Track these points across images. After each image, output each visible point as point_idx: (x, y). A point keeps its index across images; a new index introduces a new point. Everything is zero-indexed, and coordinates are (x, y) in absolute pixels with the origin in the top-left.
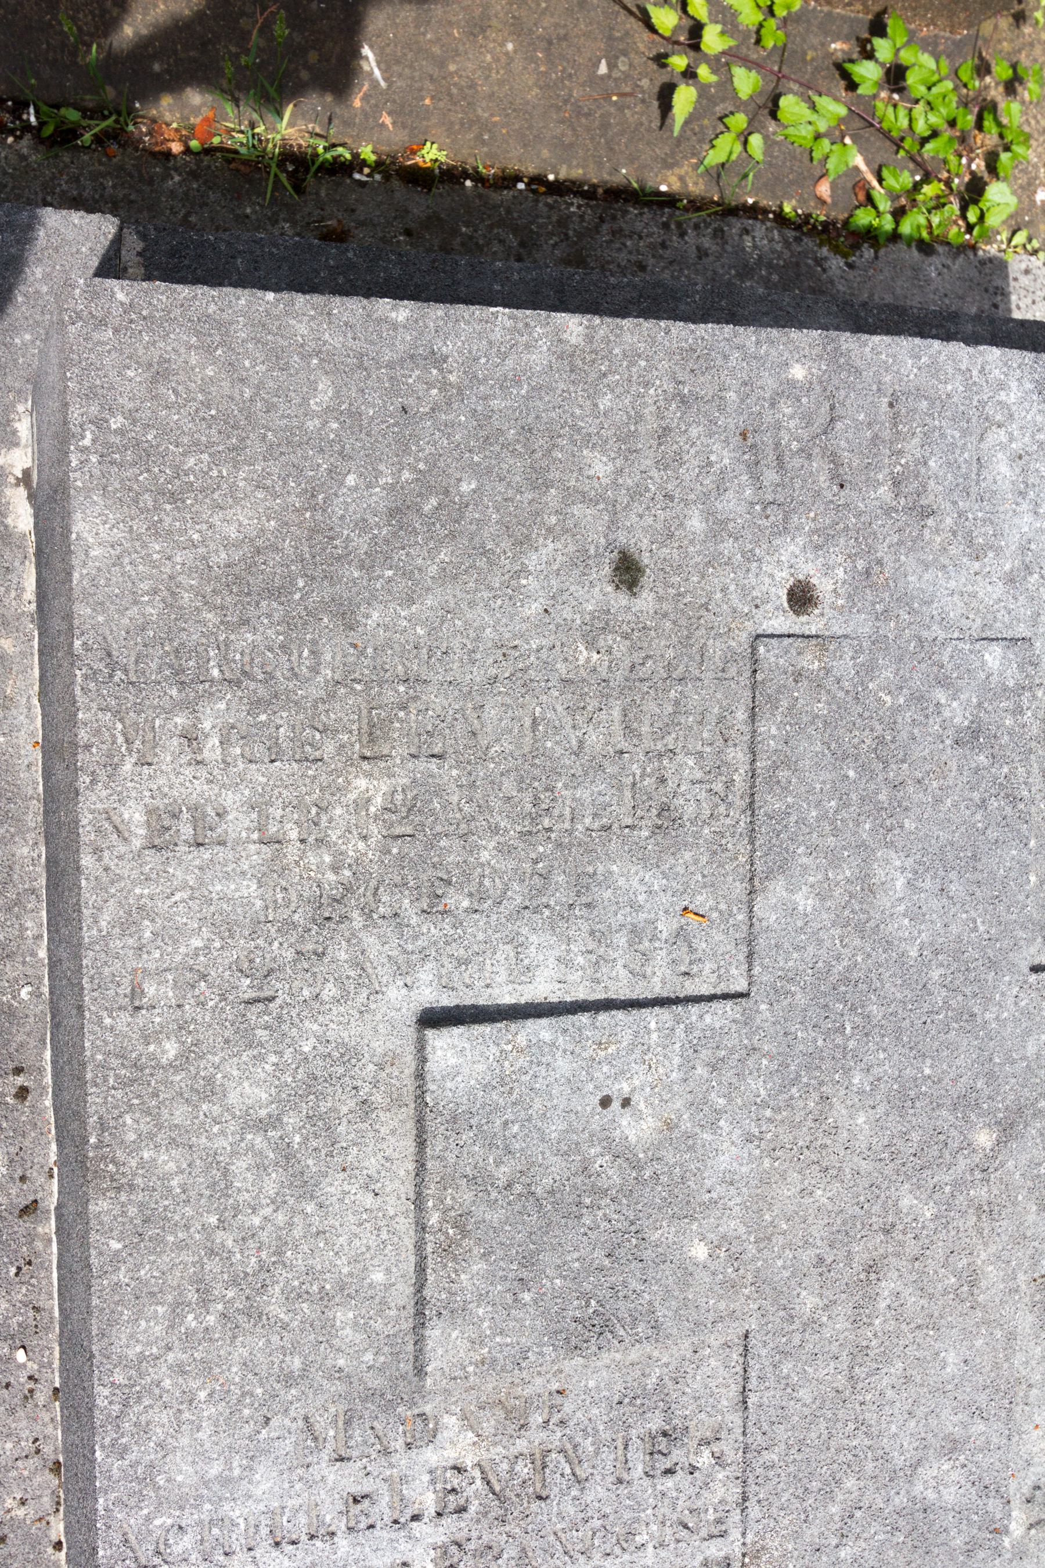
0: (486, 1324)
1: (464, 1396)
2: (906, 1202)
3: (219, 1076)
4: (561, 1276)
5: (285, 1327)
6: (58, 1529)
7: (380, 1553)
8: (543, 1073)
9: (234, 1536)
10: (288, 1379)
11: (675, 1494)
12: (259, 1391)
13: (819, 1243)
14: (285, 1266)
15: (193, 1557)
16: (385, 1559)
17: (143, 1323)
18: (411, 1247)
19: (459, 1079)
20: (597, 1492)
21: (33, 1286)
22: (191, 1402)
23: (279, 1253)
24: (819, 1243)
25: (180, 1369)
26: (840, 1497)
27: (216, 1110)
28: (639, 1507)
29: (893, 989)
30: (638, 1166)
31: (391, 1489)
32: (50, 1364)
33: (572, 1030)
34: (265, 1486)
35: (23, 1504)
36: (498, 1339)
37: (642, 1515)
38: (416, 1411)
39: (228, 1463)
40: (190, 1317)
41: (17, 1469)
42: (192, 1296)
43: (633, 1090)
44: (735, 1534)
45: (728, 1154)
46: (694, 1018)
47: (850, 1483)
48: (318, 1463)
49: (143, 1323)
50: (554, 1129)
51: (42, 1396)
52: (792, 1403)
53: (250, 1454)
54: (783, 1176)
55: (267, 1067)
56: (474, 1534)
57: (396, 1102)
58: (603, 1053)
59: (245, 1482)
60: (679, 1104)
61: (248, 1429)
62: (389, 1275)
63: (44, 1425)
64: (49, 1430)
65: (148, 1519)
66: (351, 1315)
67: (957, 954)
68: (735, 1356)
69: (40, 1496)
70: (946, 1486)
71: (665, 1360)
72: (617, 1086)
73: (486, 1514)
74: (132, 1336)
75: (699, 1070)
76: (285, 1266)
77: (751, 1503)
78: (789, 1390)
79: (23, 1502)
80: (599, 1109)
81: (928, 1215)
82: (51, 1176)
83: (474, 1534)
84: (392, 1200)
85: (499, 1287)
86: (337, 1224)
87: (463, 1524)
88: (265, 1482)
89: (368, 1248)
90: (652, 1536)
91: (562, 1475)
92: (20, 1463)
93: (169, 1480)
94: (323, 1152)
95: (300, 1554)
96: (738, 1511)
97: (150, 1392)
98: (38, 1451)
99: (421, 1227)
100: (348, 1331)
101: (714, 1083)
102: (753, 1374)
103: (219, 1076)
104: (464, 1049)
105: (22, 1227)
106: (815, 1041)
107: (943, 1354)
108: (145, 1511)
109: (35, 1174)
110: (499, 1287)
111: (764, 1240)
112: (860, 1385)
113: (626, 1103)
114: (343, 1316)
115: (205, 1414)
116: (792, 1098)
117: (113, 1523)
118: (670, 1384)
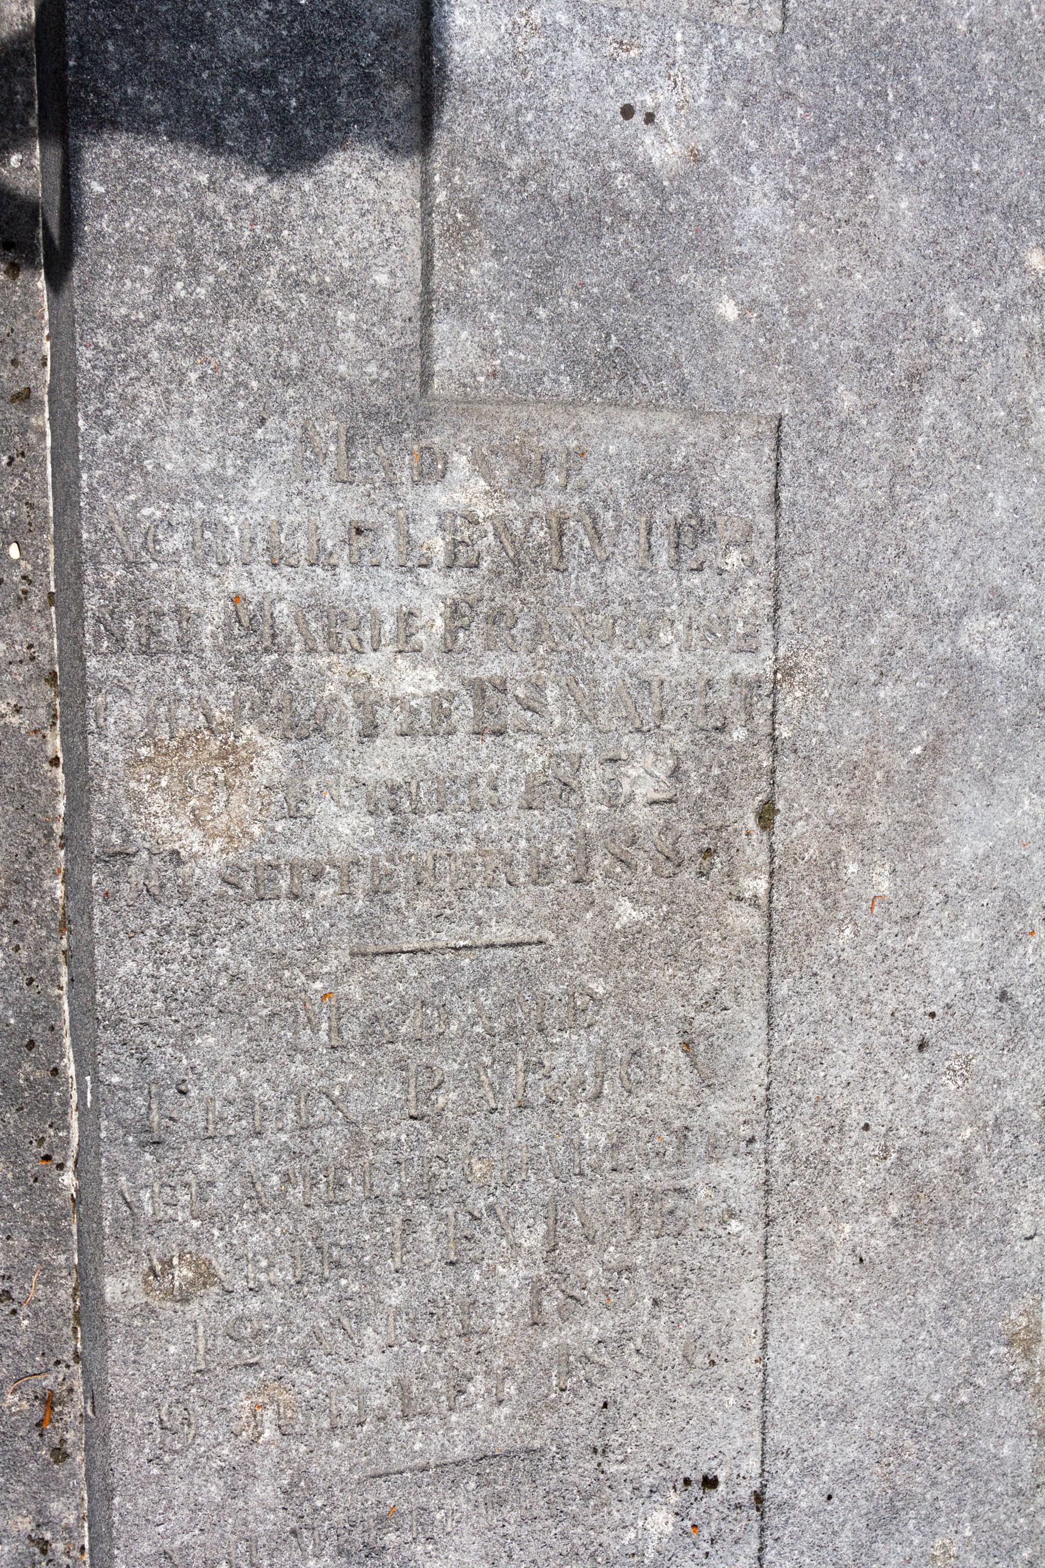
0: (497, 333)
1: (475, 435)
2: (953, 311)
3: (209, 14)
4: (578, 298)
5: (281, 315)
6: (55, 745)
7: (385, 595)
8: (559, 61)
9: (228, 546)
10: (285, 377)
11: (702, 593)
12: (254, 384)
13: (858, 335)
14: (280, 245)
15: (184, 559)
16: (391, 602)
17: (128, 282)
18: (417, 250)
19: (468, 43)
20: (617, 575)
21: (27, 480)
22: (181, 383)
23: (277, 232)
24: (858, 335)
25: (167, 343)
26: (879, 630)
27: (206, 53)
28: (663, 599)
29: (939, 63)
30: (658, 190)
31: (397, 526)
32: (45, 567)
33: (590, 19)
34: (262, 494)
35: (18, 711)
36: (511, 353)
37: (667, 610)
38: (424, 443)
39: (221, 459)
40: (179, 285)
41: (11, 673)
42: (181, 262)
43: (658, 106)
44: (767, 652)
45: (760, 208)
46: (723, 41)
47: (890, 615)
48: (318, 479)
49: (128, 282)
50: (573, 128)
51: (36, 602)
52: (828, 509)
53: (245, 454)
54: (820, 247)
55: (261, 14)
56: (487, 594)
57: (398, 73)
58: (624, 55)
59: (239, 485)
60: (707, 135)
61: (242, 426)
62: (392, 275)
63: (40, 631)
64: (45, 637)
65: (136, 506)
66: (353, 317)
67: (1009, 40)
68: (767, 450)
69: (36, 707)
70: (994, 644)
71: (691, 439)
72: (639, 98)
73: (499, 574)
74: (116, 295)
75: (729, 103)
76: (280, 245)
77: (784, 614)
78: (825, 494)
79: (17, 710)
80: (620, 118)
81: (976, 332)
82: (45, 364)
83: (487, 594)
84: (396, 194)
85: (512, 294)
86: (338, 211)
87: (474, 581)
88: (261, 488)
89: (371, 244)
90: (677, 638)
91: (581, 547)
92: (13, 668)
93: (158, 466)
94: (322, 124)
95: (300, 579)
96: (770, 626)
97: (136, 362)
98: (33, 659)
99: (427, 212)
100: (350, 335)
101: (744, 121)
102: (786, 467)
103: (209, 14)
104: (473, 11)
105: (14, 414)
106: (854, 100)
107: (991, 495)
108: (132, 497)
109: (27, 360)
110: (512, 294)
111: (799, 315)
112: (903, 508)
113: (650, 118)
114: (344, 316)
115: (197, 399)
116: (829, 160)
117: (97, 504)
118: (697, 469)
